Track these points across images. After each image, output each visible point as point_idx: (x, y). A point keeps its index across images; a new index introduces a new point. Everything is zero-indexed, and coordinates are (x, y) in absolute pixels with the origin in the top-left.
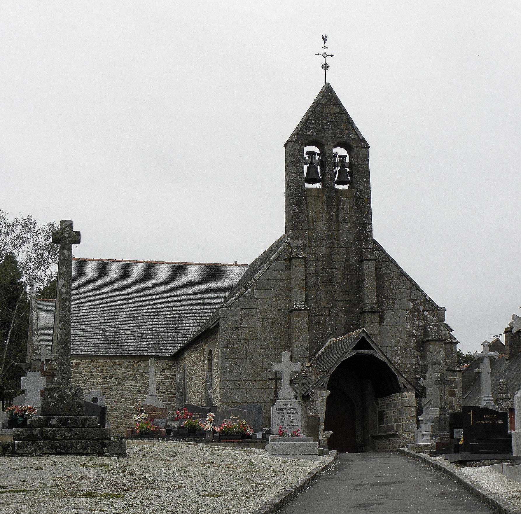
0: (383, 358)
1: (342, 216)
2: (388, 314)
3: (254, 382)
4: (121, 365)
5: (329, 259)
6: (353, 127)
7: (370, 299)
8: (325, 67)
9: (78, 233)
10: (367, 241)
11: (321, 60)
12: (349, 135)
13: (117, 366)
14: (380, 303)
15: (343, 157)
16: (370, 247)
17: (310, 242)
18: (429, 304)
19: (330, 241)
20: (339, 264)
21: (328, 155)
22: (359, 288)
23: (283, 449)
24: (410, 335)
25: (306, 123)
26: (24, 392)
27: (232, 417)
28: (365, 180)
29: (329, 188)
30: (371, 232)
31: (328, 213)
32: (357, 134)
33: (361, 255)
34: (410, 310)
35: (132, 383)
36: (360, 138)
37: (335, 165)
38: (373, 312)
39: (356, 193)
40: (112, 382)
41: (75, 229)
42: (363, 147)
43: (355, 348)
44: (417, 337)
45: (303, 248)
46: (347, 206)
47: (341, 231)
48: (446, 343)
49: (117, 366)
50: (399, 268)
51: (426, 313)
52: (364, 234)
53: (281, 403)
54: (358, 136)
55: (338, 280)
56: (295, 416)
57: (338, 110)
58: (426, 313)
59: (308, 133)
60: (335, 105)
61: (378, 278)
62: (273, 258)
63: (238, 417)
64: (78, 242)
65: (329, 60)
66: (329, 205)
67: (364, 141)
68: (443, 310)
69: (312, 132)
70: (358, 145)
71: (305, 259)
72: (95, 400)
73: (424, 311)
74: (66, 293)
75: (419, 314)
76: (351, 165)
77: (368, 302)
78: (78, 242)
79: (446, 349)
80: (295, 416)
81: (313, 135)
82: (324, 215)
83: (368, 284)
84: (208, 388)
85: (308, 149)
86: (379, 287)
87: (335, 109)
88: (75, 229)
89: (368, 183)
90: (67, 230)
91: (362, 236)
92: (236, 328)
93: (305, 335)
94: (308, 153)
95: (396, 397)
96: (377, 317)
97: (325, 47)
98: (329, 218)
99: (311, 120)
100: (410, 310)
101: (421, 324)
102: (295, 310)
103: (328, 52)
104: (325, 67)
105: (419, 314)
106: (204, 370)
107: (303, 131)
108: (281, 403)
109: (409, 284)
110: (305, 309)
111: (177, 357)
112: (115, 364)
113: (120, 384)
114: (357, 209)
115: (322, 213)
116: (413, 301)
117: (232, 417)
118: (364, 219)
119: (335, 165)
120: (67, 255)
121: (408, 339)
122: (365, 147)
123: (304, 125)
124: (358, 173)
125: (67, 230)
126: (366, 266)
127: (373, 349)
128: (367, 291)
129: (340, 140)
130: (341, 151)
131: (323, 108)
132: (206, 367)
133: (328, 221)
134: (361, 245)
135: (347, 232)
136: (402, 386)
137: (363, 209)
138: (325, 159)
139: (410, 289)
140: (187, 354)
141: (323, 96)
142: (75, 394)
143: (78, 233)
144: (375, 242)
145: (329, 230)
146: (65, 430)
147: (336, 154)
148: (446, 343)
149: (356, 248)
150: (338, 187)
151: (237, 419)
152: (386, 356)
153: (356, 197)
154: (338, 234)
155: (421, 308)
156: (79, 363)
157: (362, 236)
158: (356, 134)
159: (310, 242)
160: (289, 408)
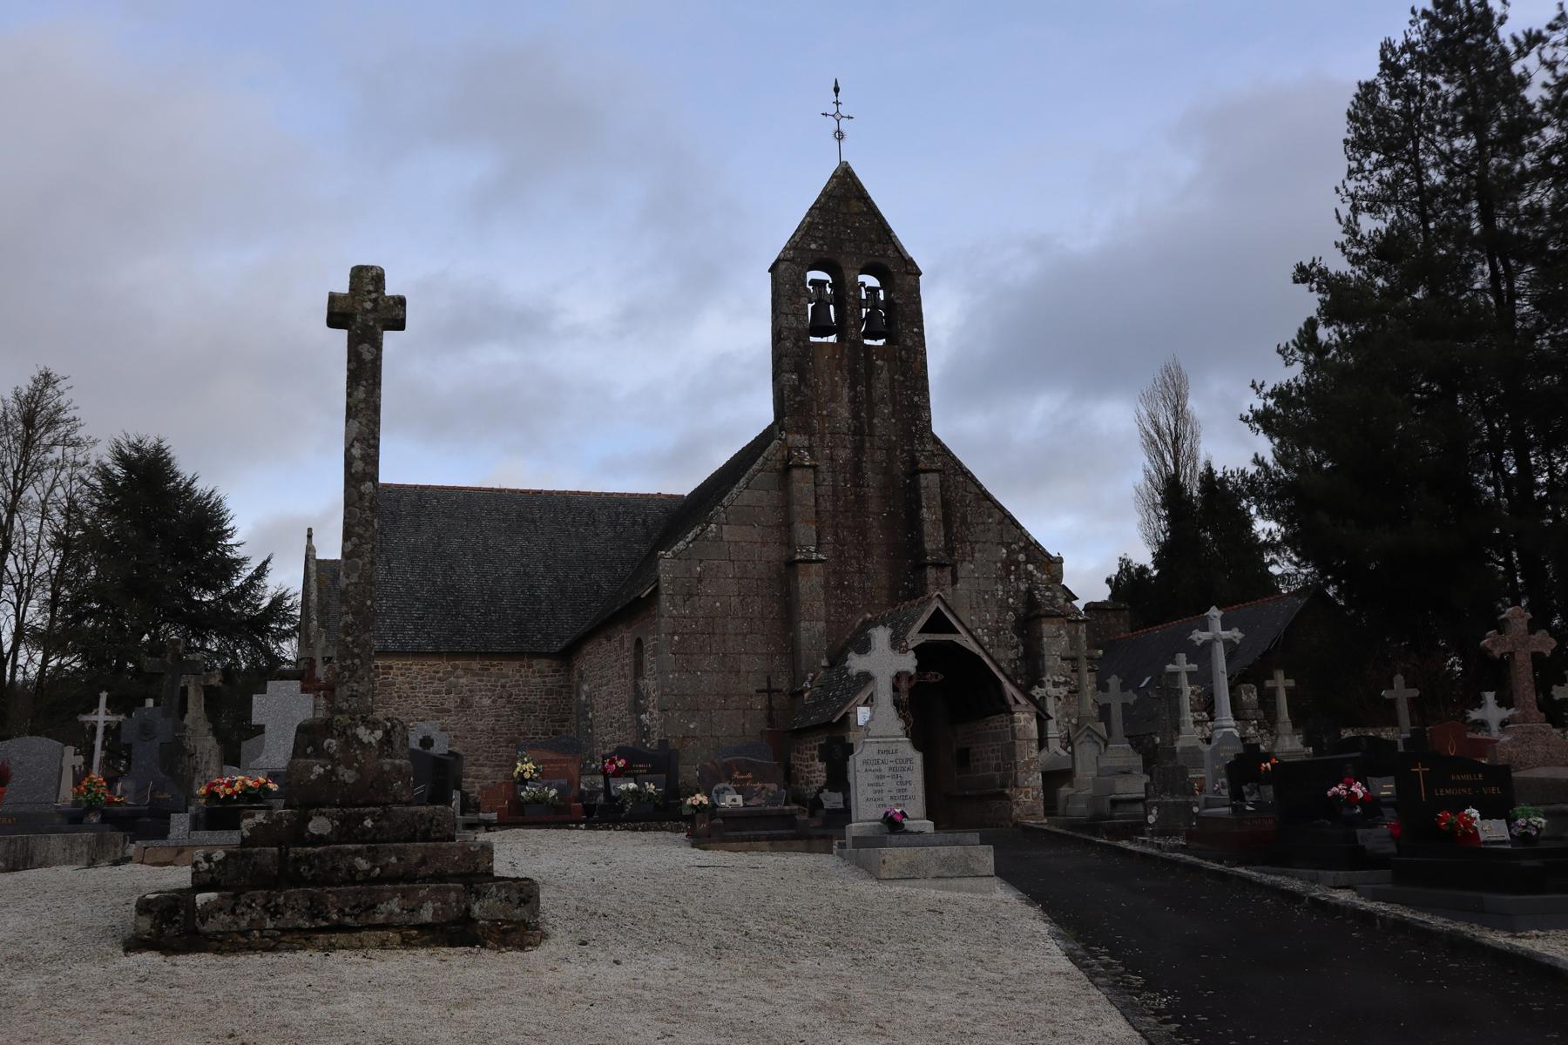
0: (976, 649)
2: (965, 569)
3: (726, 697)
4: (466, 670)
5: (857, 470)
7: (933, 540)
8: (839, 135)
9: (401, 302)
10: (922, 437)
12: (885, 251)
13: (460, 672)
14: (950, 550)
15: (873, 291)
16: (928, 447)
17: (822, 439)
18: (1034, 551)
20: (872, 479)
21: (846, 286)
22: (913, 522)
23: (910, 865)
24: (1003, 606)
25: (807, 230)
26: (260, 729)
27: (736, 775)
29: (850, 347)
31: (853, 387)
33: (914, 461)
34: (1003, 562)
35: (486, 702)
37: (861, 304)
38: (939, 566)
40: (451, 702)
41: (391, 289)
43: (922, 631)
44: (1015, 610)
45: (810, 449)
46: (885, 375)
48: (1070, 621)
49: (460, 672)
50: (980, 486)
51: (1030, 567)
53: (875, 747)
55: (873, 506)
56: (907, 776)
58: (1030, 567)
59: (813, 246)
61: (946, 504)
62: (755, 467)
63: (749, 776)
64: (399, 325)
68: (1060, 561)
70: (900, 273)
71: (814, 467)
72: (427, 742)
73: (1027, 562)
74: (363, 458)
75: (1017, 568)
76: (889, 304)
77: (928, 546)
78: (399, 325)
79: (1068, 633)
80: (907, 776)
83: (930, 515)
84: (637, 708)
85: (813, 275)
86: (947, 520)
87: (856, 206)
88: (391, 289)
90: (369, 292)
92: (691, 595)
93: (819, 608)
94: (813, 282)
95: (997, 721)
96: (947, 572)
97: (837, 103)
98: (855, 396)
100: (1003, 562)
101: (1023, 587)
102: (801, 561)
103: (843, 110)
104: (839, 135)
105: (1017, 568)
106: (625, 676)
108: (875, 747)
109: (998, 515)
110: (819, 561)
111: (567, 655)
112: (455, 668)
113: (465, 704)
116: (1008, 546)
117: (736, 775)
119: (861, 304)
120: (368, 356)
121: (1000, 613)
124: (900, 314)
125: (369, 292)
126: (923, 483)
127: (957, 632)
128: (927, 528)
130: (871, 281)
132: (628, 670)
133: (853, 400)
134: (912, 445)
135: (884, 421)
136: (1012, 702)
138: (843, 291)
139: (1000, 523)
140: (588, 648)
141: (838, 183)
142: (387, 740)
143: (401, 302)
144: (936, 441)
146: (357, 853)
147: (863, 284)
148: (1070, 621)
149: (903, 451)
150: (867, 342)
151: (746, 780)
152: (982, 647)
153: (901, 360)
154: (871, 426)
155: (1022, 557)
156: (391, 668)
160: (893, 757)
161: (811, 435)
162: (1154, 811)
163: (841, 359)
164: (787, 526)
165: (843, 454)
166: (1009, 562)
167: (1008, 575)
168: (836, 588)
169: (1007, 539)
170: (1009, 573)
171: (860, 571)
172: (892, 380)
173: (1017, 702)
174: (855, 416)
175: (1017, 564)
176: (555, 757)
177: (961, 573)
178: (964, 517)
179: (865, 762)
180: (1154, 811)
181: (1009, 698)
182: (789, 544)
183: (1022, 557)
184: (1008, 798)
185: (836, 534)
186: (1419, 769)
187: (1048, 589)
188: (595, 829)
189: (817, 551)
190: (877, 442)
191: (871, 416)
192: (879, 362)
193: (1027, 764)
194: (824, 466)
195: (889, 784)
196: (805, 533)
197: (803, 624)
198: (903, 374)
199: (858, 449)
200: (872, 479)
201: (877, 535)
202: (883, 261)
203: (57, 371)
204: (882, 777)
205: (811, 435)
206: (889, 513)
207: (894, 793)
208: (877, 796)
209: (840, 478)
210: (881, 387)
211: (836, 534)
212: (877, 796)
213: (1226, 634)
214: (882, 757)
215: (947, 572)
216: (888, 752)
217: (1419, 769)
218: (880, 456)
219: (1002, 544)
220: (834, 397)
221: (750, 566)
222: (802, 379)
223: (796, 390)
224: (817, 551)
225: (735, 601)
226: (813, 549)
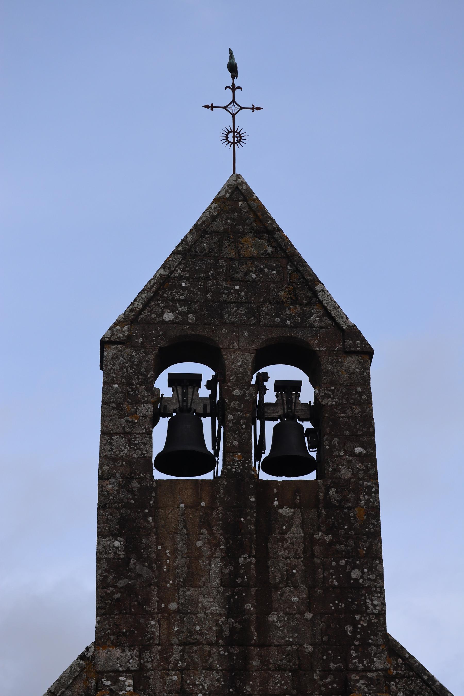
1: (277, 569)
6: (315, 293)
8: (235, 137)
10: (365, 644)
11: (223, 120)
12: (304, 317)
16: (378, 663)
17: (165, 656)
19: (236, 650)
28: (358, 450)
30: (382, 614)
31: (230, 557)
32: (331, 314)
36: (338, 325)
39: (327, 493)
42: (350, 353)
46: (295, 533)
47: (273, 618)
52: (355, 624)
54: (333, 319)
57: (270, 250)
59: (169, 316)
60: (258, 233)
65: (244, 121)
66: (233, 530)
67: (354, 333)
69: (180, 314)
70: (338, 352)
81: (185, 322)
82: (216, 566)
87: (251, 245)
89: (370, 458)
91: (349, 628)
97: (233, 88)
98: (235, 574)
99: (180, 278)
103: (230, 91)
104: (235, 137)
107: (151, 312)
114: (331, 543)
115: (210, 558)
118: (355, 574)
119: (264, 412)
122: (356, 353)
123: (156, 293)
129: (276, 333)
131: (220, 246)
133: (229, 582)
134: (346, 659)
135: (289, 621)
137: (351, 542)
141: (220, 211)
144: (395, 650)
145: (229, 613)
149: (326, 672)
153: (329, 505)
154: (264, 627)
157: (349, 628)
158: (328, 314)
159: (165, 656)
163: (211, 507)
172: (310, 541)
174: (233, 609)
190: (275, 657)
192: (285, 511)
198: (331, 530)
210: (286, 556)
220: (192, 578)
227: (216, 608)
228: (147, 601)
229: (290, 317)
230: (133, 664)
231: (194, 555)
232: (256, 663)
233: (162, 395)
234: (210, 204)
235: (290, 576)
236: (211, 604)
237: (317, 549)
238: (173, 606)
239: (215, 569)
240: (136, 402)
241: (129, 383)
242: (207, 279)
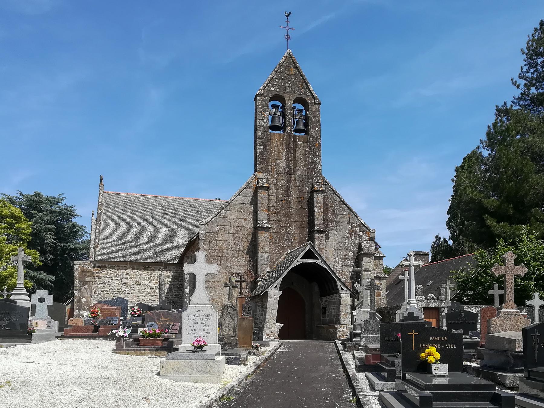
1: (298, 158)
2: (332, 233)
5: (288, 189)
7: (319, 221)
10: (317, 176)
11: (285, 31)
14: (326, 224)
19: (289, 175)
20: (294, 193)
24: (348, 249)
31: (287, 153)
34: (349, 231)
43: (302, 258)
45: (267, 180)
46: (302, 149)
47: (297, 168)
51: (361, 233)
55: (294, 205)
56: (209, 323)
58: (361, 233)
59: (273, 89)
61: (325, 205)
63: (168, 319)
65: (291, 32)
66: (288, 146)
73: (360, 231)
75: (355, 233)
83: (318, 210)
86: (326, 212)
87: (293, 71)
95: (334, 296)
98: (288, 157)
100: (349, 231)
105: (355, 233)
113: (137, 283)
128: (316, 215)
129: (298, 96)
133: (287, 159)
136: (340, 289)
151: (166, 321)
153: (310, 142)
154: (295, 171)
155: (357, 229)
160: (203, 314)
161: (268, 173)
162: (364, 340)
163: (283, 140)
164: (255, 212)
165: (282, 182)
166: (352, 231)
167: (351, 237)
168: (276, 239)
169: (351, 221)
170: (351, 236)
171: (287, 233)
172: (305, 151)
173: (342, 289)
174: (288, 166)
175: (356, 232)
176: (109, 307)
177: (330, 235)
178: (333, 211)
179: (188, 316)
180: (364, 340)
181: (339, 287)
182: (256, 220)
183: (357, 229)
184: (336, 328)
185: (277, 217)
186: (413, 334)
187: (368, 243)
188: (107, 340)
189: (268, 223)
190: (297, 178)
191: (295, 166)
192: (300, 143)
193: (345, 315)
194: (272, 187)
195: (200, 327)
196: (263, 216)
197: (259, 254)
198: (310, 148)
199: (289, 181)
200: (294, 193)
201: (295, 217)
202: (304, 97)
203: (437, 235)
204: (197, 323)
205: (268, 173)
206: (301, 208)
207: (202, 331)
208: (193, 332)
209: (280, 193)
210: (300, 153)
211: (277, 217)
212: (193, 332)
213: (416, 263)
214: (197, 313)
215: (324, 236)
216: (200, 311)
217: (413, 334)
218: (298, 184)
219: (349, 223)
220: (279, 158)
221: (239, 229)
222: (265, 149)
223: (262, 154)
224: (268, 223)
225: (232, 243)
226: (265, 222)
227: (284, 165)
228: (268, 162)
229: (302, 92)
230: (266, 177)
231: (279, 152)
232: (293, 179)
233: (50, 294)
234: (526, 45)
235: (301, 159)
236: (283, 164)
237: (307, 153)
238: (274, 164)
239: (284, 156)
240: (265, 111)
241: (263, 106)
242: (282, 79)
